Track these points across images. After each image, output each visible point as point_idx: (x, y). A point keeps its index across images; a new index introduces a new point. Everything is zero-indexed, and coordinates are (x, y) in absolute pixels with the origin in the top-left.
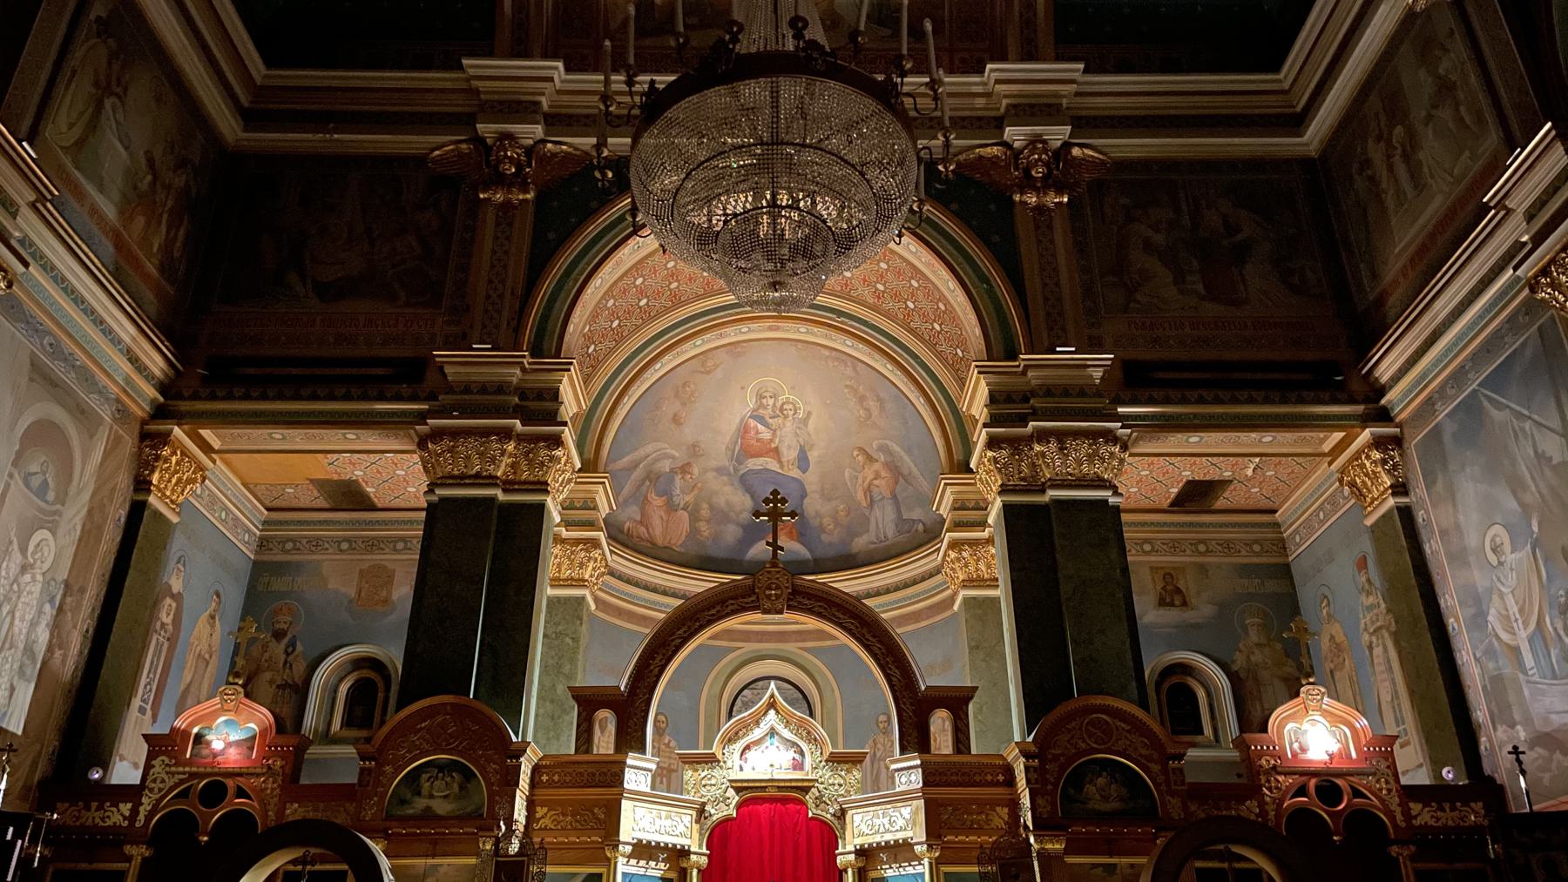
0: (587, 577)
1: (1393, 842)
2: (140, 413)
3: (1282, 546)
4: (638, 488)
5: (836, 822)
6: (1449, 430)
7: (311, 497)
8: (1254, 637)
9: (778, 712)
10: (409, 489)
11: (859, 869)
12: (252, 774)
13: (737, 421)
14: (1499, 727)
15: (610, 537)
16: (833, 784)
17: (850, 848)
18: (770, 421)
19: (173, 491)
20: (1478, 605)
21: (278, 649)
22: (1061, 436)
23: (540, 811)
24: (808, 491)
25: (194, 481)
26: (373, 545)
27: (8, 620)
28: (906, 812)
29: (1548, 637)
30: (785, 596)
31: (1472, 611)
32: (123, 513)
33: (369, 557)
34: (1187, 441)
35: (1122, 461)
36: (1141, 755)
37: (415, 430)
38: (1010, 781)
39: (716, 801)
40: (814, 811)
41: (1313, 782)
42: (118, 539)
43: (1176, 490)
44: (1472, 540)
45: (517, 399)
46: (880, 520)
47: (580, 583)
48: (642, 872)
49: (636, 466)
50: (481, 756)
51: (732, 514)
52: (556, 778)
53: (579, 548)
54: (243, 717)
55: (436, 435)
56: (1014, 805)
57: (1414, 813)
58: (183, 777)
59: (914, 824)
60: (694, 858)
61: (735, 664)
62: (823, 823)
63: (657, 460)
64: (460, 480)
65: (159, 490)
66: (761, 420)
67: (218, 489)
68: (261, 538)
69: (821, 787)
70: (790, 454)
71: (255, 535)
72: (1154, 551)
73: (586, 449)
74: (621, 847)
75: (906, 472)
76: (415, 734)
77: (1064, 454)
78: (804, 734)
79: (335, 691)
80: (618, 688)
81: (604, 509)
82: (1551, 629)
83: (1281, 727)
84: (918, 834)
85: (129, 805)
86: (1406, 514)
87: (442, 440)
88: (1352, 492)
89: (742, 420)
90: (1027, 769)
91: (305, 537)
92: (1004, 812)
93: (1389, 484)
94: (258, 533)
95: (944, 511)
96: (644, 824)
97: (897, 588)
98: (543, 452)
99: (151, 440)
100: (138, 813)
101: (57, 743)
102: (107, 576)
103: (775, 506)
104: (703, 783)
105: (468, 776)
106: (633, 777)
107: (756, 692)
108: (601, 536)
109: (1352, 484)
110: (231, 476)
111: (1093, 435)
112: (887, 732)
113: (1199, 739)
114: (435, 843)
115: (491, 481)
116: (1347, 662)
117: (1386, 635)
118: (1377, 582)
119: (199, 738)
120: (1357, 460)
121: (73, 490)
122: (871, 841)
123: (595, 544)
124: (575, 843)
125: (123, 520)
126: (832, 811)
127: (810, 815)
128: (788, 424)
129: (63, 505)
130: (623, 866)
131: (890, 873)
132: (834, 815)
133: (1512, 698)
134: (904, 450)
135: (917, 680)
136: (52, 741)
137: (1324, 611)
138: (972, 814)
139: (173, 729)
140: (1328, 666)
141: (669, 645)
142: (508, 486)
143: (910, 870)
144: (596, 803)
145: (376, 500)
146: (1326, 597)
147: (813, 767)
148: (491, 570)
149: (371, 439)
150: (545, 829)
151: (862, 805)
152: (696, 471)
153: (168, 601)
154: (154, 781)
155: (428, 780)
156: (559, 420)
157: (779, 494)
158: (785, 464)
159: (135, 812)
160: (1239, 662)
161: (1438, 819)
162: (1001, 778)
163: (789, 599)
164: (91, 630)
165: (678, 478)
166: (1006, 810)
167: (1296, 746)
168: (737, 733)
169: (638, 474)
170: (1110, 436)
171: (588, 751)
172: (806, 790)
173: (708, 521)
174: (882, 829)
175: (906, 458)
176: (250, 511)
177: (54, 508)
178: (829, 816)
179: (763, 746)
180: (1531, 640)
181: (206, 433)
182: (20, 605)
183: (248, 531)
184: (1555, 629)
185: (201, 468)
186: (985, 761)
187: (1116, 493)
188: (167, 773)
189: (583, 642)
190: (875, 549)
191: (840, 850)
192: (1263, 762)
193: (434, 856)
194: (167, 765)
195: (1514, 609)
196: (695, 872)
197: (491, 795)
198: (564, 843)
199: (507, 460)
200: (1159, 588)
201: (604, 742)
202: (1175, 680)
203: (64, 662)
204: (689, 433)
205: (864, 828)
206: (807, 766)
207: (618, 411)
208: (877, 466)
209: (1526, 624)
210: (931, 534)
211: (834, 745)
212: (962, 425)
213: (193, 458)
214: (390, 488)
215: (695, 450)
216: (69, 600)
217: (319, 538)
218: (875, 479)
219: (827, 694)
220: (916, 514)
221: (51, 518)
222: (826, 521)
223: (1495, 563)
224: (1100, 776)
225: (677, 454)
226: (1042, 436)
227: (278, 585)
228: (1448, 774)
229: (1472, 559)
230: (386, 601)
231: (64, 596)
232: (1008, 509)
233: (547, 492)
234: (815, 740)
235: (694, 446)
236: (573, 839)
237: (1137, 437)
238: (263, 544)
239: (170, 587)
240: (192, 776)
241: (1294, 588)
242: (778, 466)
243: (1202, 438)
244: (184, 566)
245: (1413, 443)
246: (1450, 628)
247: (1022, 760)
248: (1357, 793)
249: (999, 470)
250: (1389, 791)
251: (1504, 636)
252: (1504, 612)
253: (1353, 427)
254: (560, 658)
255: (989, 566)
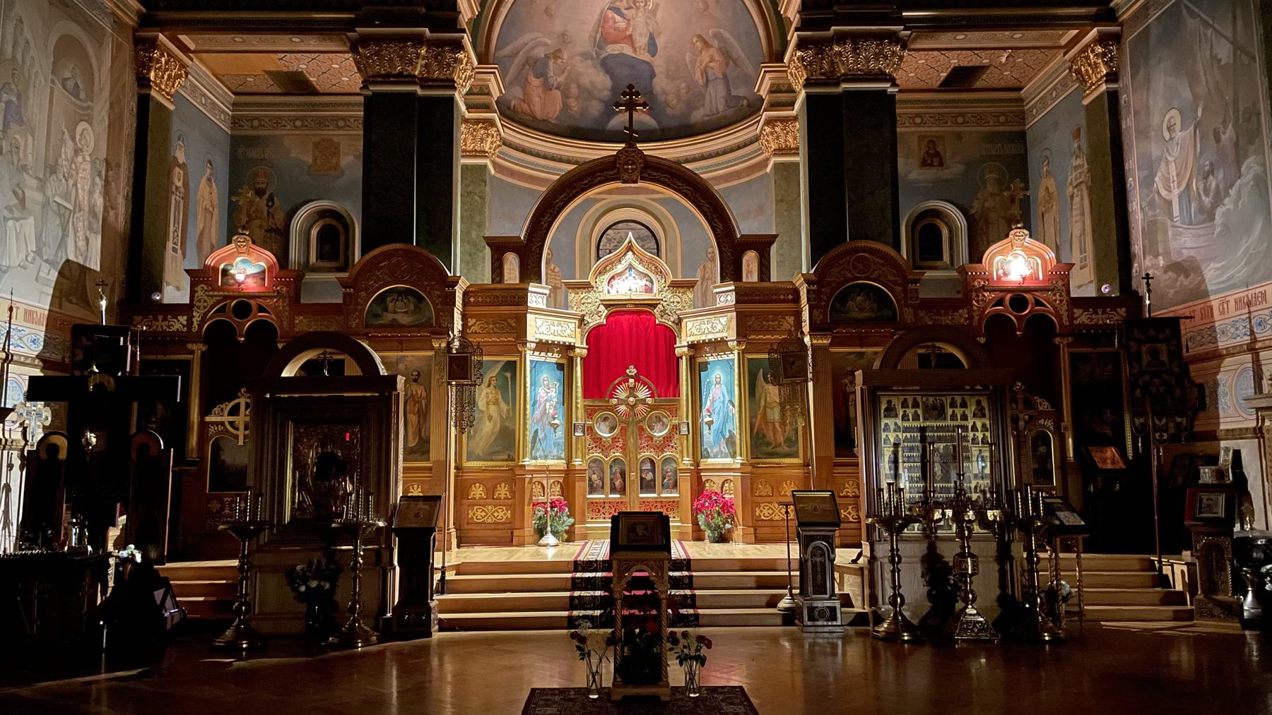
0: (487, 149)
1: (1059, 335)
2: (131, 23)
3: (1022, 117)
4: (520, 72)
5: (675, 327)
6: (1155, 32)
7: (268, 85)
8: (990, 188)
9: (634, 253)
10: (343, 79)
11: (690, 356)
12: (268, 297)
13: (598, 12)
14: (1147, 257)
15: (503, 114)
16: (671, 303)
17: (685, 343)
18: (625, 12)
19: (166, 85)
20: (1150, 168)
21: (262, 203)
22: (856, 38)
23: (471, 322)
24: (656, 71)
25: (179, 76)
26: (321, 123)
27: (74, 190)
28: (723, 320)
29: (1192, 194)
30: (639, 170)
31: (1146, 172)
32: (134, 104)
33: (319, 132)
34: (955, 38)
35: (901, 58)
36: (889, 281)
37: (347, 36)
38: (797, 299)
39: (592, 314)
40: (660, 320)
41: (1009, 296)
42: (135, 125)
43: (945, 74)
44: (1155, 120)
45: (424, 10)
46: (713, 95)
47: (483, 154)
48: (543, 359)
49: (517, 53)
50: (427, 285)
51: (596, 92)
52: (480, 299)
53: (480, 126)
54: (253, 258)
55: (365, 41)
56: (798, 315)
57: (1075, 316)
58: (218, 298)
59: (729, 328)
60: (578, 350)
61: (602, 210)
62: (666, 328)
63: (533, 48)
64: (386, 79)
65: (157, 85)
66: (617, 11)
67: (196, 79)
68: (233, 117)
69: (665, 304)
70: (642, 41)
71: (228, 114)
72: (923, 123)
73: (478, 42)
74: (528, 344)
75: (734, 56)
76: (379, 270)
77: (857, 54)
78: (653, 268)
79: (309, 234)
80: (519, 238)
81: (496, 94)
82: (1195, 189)
83: (992, 259)
84: (731, 335)
85: (185, 318)
86: (1113, 97)
87: (369, 45)
88: (1078, 79)
89: (602, 12)
90: (808, 291)
91: (268, 116)
92: (791, 319)
93: (1105, 72)
94: (230, 113)
95: (763, 93)
96: (543, 329)
97: (725, 152)
98: (448, 55)
99: (143, 46)
100: (193, 323)
101: (123, 276)
102: (133, 154)
103: (631, 97)
104: (583, 301)
105: (420, 299)
106: (534, 299)
107: (617, 231)
108: (495, 116)
109: (1078, 72)
110: (204, 68)
111: (879, 37)
112: (713, 260)
113: (939, 263)
114: (401, 342)
115: (411, 80)
116: (1054, 208)
117: (1084, 188)
118: (1085, 149)
119: (225, 272)
120: (1084, 53)
121: (96, 89)
122: (699, 339)
123: (491, 123)
124: (496, 342)
125: (135, 110)
126: (672, 319)
127: (657, 322)
128: (640, 14)
129: (92, 102)
130: (530, 356)
131: (711, 359)
132: (673, 322)
133: (1160, 237)
134: (734, 38)
135: (734, 230)
136: (121, 275)
137: (1045, 169)
138: (769, 321)
139: (205, 266)
140: (1042, 209)
141: (554, 207)
142: (425, 82)
143: (725, 357)
144: (509, 316)
145: (318, 87)
146: (1047, 158)
147: (659, 291)
148: (417, 149)
149: (312, 43)
150: (475, 333)
151: (694, 315)
152: (565, 56)
153: (177, 169)
154: (199, 301)
155: (392, 302)
156: (459, 27)
157: (634, 88)
158: (638, 50)
159: (190, 322)
160: (976, 208)
161: (1092, 320)
162: (790, 297)
163: (642, 172)
164: (130, 194)
165: (551, 63)
166: (792, 318)
167: (1001, 272)
168: (605, 268)
169: (519, 59)
170: (894, 38)
171: (501, 281)
172: (654, 306)
173: (576, 99)
174: (706, 331)
175: (736, 44)
176: (224, 98)
177: (85, 105)
178: (670, 323)
179: (624, 277)
180: (1180, 197)
181: (184, 38)
182: (79, 180)
183: (223, 111)
184: (1198, 189)
185: (183, 66)
186: (780, 286)
187: (894, 84)
188: (207, 296)
189: (487, 200)
190: (708, 121)
191: (678, 345)
192: (976, 283)
193: (402, 350)
194: (206, 290)
195: (1173, 172)
196: (579, 359)
197: (437, 311)
198: (489, 342)
199: (422, 62)
200: (923, 151)
201: (512, 271)
202: (925, 222)
203: (116, 218)
204: (558, 25)
205: (694, 330)
206: (655, 290)
207: (502, 9)
208: (713, 51)
209: (1179, 184)
210: (752, 108)
211: (675, 274)
212: (782, 24)
213: (177, 59)
214: (328, 78)
215: (564, 38)
216: (110, 173)
217: (279, 117)
218: (710, 62)
219: (670, 234)
220: (741, 92)
221: (86, 113)
222: (671, 97)
223: (1167, 137)
224: (859, 295)
225: (549, 42)
226: (841, 38)
227: (253, 154)
228: (1105, 289)
229: (1153, 133)
230: (336, 166)
231: (107, 171)
232: (809, 97)
233: (455, 88)
234: (661, 272)
235: (563, 34)
236: (494, 339)
237: (916, 36)
238: (235, 122)
239: (176, 159)
240: (225, 298)
241: (1026, 151)
242: (631, 50)
243: (967, 36)
244: (183, 142)
245: (1128, 41)
246: (1128, 185)
247: (806, 285)
248: (1038, 303)
249: (805, 67)
250: (1061, 301)
251: (1164, 193)
252: (1166, 175)
253: (1085, 25)
254: (471, 211)
255: (795, 139)
